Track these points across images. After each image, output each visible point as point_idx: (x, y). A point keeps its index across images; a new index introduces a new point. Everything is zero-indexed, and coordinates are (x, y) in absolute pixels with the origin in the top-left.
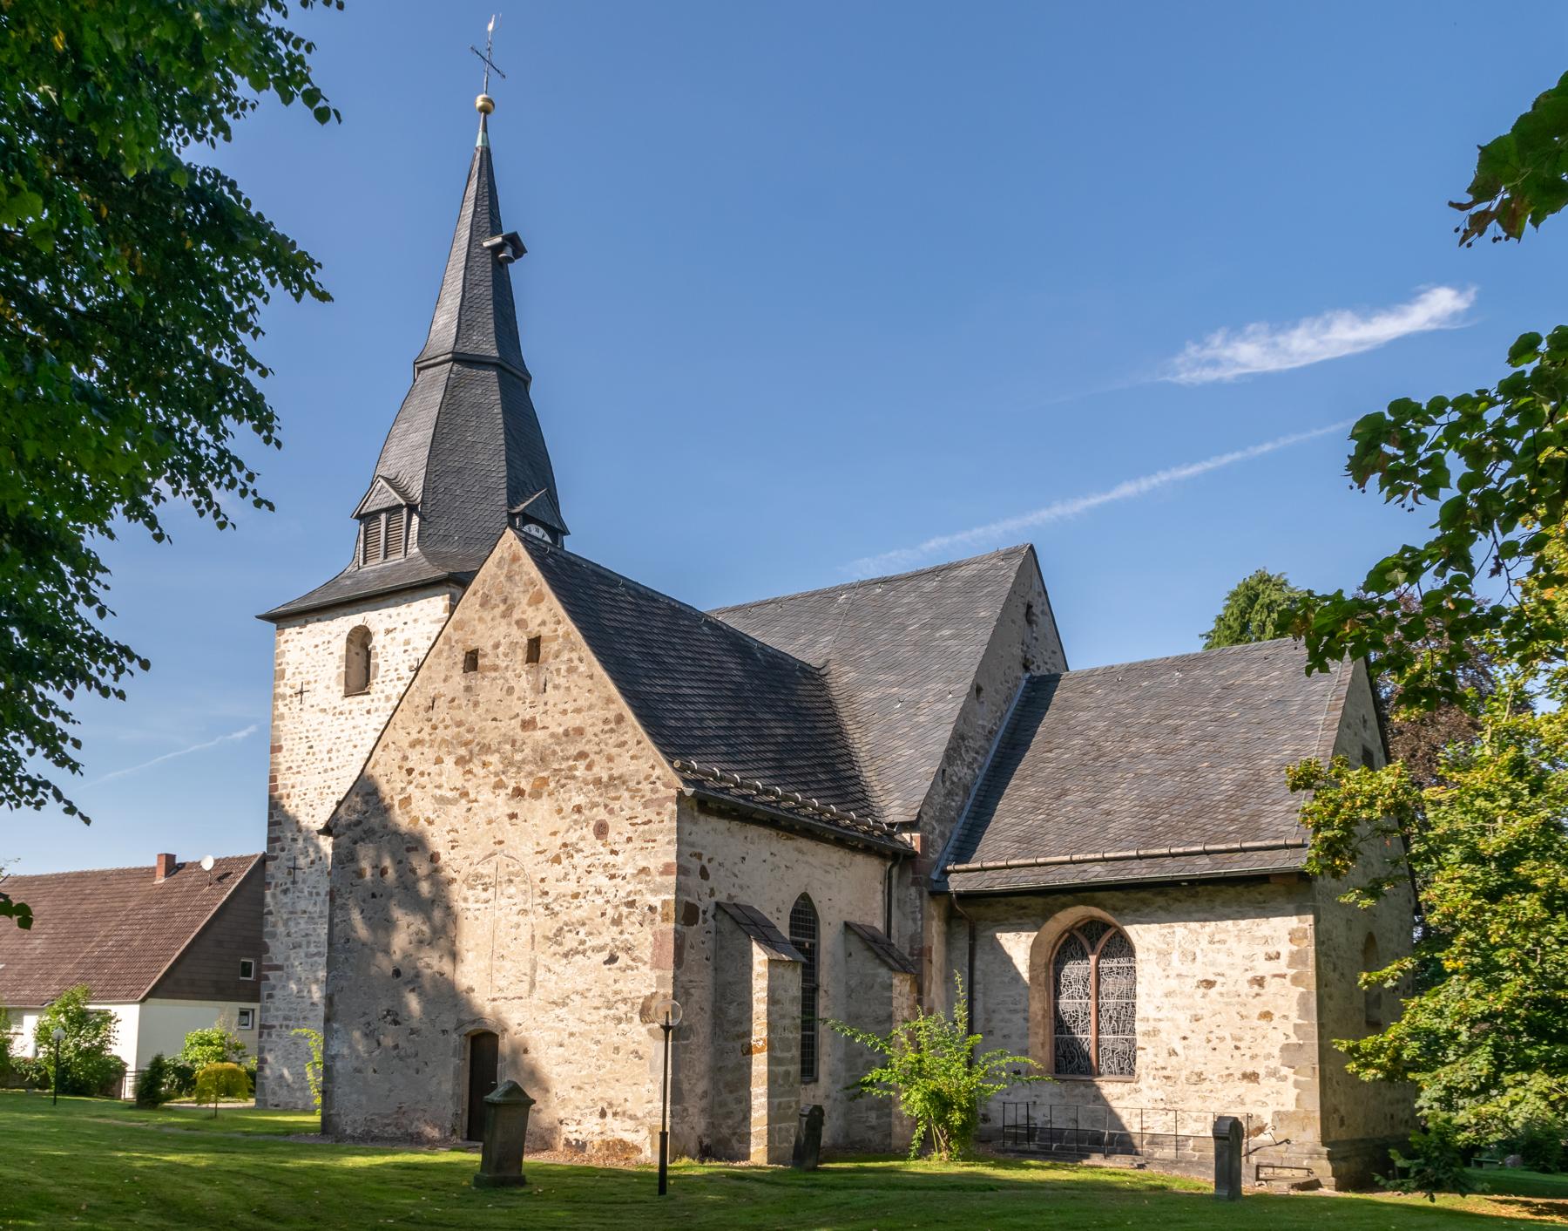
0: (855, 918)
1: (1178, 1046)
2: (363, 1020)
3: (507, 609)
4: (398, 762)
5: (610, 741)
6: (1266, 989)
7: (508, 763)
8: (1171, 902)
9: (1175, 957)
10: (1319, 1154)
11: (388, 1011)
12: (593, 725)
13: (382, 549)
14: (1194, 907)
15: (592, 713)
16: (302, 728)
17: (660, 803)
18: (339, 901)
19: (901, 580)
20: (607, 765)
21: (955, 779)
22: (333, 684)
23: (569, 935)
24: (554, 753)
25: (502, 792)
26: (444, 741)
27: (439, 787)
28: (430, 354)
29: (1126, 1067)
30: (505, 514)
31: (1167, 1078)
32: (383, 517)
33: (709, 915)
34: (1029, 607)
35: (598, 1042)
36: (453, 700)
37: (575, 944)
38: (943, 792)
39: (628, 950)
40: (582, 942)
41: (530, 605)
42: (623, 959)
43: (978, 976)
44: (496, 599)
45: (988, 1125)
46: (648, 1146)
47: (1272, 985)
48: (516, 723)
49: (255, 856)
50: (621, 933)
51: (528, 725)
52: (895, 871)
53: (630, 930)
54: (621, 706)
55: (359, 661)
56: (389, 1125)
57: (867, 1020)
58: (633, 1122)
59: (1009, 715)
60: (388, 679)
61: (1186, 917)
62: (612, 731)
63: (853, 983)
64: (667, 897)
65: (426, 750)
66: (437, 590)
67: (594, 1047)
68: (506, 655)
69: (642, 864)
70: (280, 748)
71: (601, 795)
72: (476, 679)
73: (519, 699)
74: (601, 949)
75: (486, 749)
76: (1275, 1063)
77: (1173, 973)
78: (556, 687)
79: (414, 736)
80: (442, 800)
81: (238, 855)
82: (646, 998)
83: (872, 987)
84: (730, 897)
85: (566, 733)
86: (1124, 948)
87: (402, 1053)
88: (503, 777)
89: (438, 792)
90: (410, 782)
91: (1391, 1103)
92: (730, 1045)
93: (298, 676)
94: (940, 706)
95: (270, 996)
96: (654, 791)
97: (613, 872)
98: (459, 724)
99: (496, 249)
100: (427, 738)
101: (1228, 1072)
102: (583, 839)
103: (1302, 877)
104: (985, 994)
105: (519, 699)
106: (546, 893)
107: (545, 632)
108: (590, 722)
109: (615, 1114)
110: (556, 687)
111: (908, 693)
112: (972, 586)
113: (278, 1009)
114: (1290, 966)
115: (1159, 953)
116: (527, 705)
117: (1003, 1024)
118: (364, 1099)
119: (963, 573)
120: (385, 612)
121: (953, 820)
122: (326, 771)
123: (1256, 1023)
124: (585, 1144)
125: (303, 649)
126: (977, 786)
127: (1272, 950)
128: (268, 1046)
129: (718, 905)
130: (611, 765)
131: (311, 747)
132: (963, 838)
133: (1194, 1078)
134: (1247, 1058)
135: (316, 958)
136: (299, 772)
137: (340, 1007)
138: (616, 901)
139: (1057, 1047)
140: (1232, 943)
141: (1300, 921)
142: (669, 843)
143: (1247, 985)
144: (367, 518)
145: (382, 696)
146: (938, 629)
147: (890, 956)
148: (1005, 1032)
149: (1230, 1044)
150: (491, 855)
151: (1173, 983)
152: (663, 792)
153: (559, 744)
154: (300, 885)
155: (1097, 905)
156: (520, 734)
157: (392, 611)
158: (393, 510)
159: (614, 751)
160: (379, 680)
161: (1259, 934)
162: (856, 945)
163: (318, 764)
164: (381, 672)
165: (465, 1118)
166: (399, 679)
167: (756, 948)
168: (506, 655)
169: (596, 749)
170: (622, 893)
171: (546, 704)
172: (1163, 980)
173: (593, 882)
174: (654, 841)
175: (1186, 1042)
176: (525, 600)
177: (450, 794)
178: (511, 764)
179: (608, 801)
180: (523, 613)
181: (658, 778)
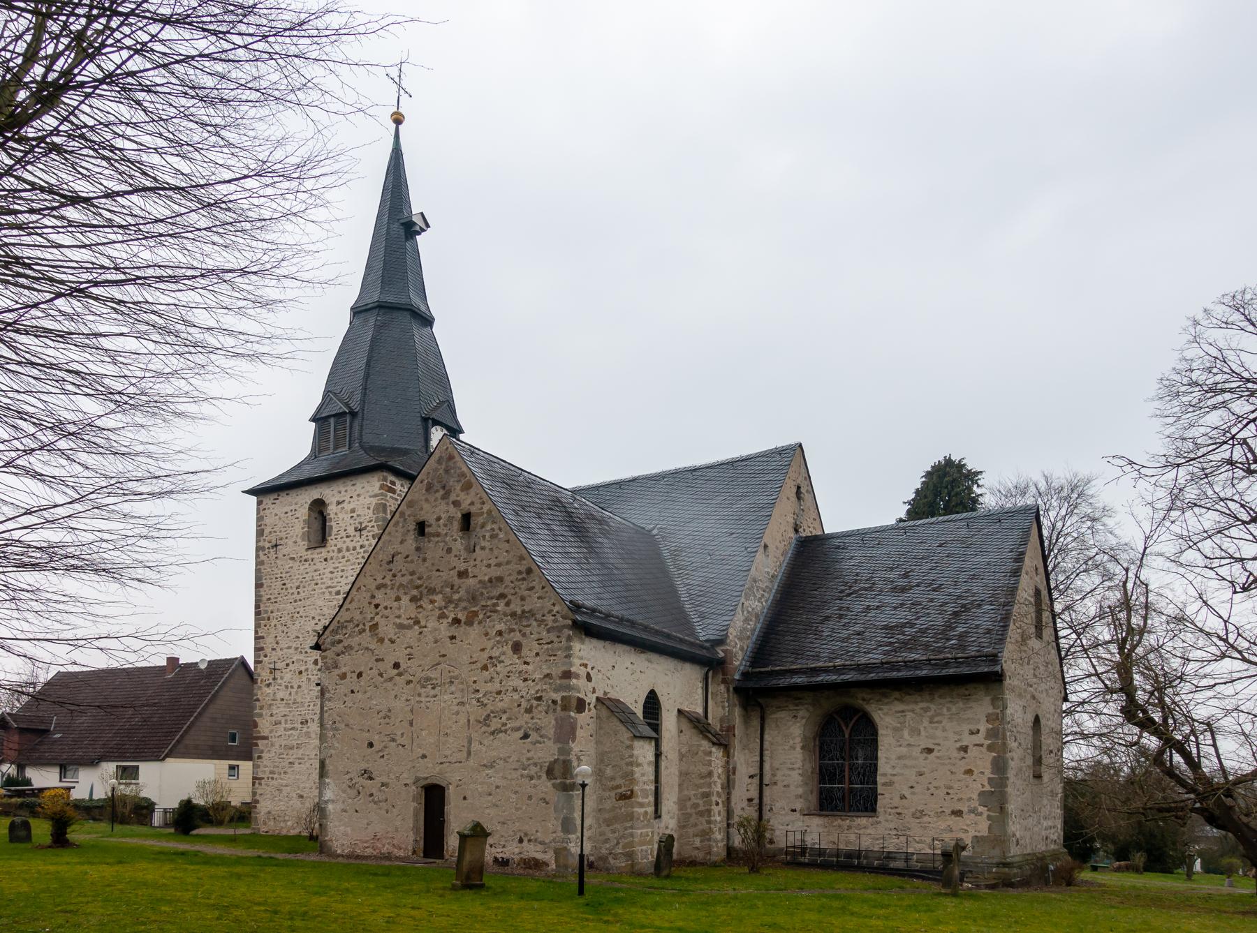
1: (907, 793)
2: (347, 777)
4: (368, 599)
7: (449, 601)
11: (365, 771)
12: (510, 575)
14: (919, 699)
16: (276, 571)
17: (560, 629)
21: (750, 609)
22: (299, 540)
23: (495, 720)
24: (482, 594)
25: (445, 621)
26: (401, 585)
27: (399, 617)
31: (899, 814)
32: (332, 420)
33: (592, 706)
34: (799, 488)
35: (516, 792)
36: (407, 557)
37: (499, 726)
38: (742, 618)
39: (537, 730)
40: (504, 725)
41: (462, 490)
42: (534, 736)
43: (766, 745)
44: (437, 486)
45: (773, 846)
47: (974, 751)
48: (454, 573)
50: (532, 718)
51: (463, 574)
52: (710, 674)
55: (317, 525)
60: (339, 537)
62: (524, 579)
65: (388, 591)
67: (514, 796)
68: (445, 525)
71: (516, 624)
73: (456, 556)
74: (518, 729)
75: (432, 591)
76: (975, 804)
78: (483, 548)
79: (380, 581)
80: (401, 627)
82: (550, 762)
83: (697, 753)
84: (605, 693)
85: (490, 580)
87: (376, 799)
89: (398, 621)
90: (377, 614)
91: (1046, 829)
95: (260, 757)
100: (389, 583)
102: (504, 653)
104: (771, 757)
106: (478, 691)
107: (473, 509)
108: (507, 573)
109: (530, 841)
110: (483, 548)
113: (266, 766)
116: (462, 560)
118: (349, 829)
121: (748, 638)
122: (295, 601)
124: (508, 860)
127: (974, 728)
128: (259, 792)
129: (598, 699)
130: (523, 603)
131: (284, 584)
137: (330, 767)
139: (821, 793)
143: (956, 751)
145: (335, 549)
147: (709, 732)
148: (785, 783)
151: (904, 750)
152: (561, 622)
154: (279, 681)
156: (457, 581)
160: (333, 537)
162: (685, 725)
163: (289, 596)
164: (334, 531)
165: (422, 843)
168: (445, 525)
169: (513, 591)
173: (511, 683)
176: (458, 487)
177: (406, 622)
178: (450, 601)
179: (522, 628)
180: (457, 496)
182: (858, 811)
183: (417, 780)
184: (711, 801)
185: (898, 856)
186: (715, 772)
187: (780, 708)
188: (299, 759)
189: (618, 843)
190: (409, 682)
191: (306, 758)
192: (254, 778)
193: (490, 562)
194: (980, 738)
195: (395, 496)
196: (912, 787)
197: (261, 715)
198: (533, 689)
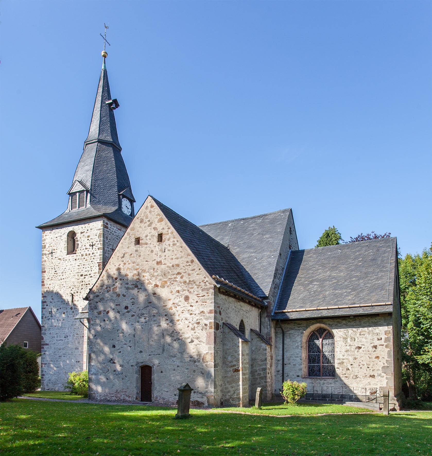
0: (253, 328)
3: (150, 224)
5: (189, 269)
6: (377, 349)
8: (347, 322)
9: (349, 340)
10: (394, 399)
12: (183, 263)
13: (78, 205)
15: (182, 259)
17: (208, 289)
18: (92, 322)
19: (249, 219)
20: (188, 277)
21: (276, 283)
22: (63, 250)
24: (169, 273)
28: (90, 139)
29: (331, 374)
30: (117, 194)
32: (78, 194)
34: (290, 228)
35: (187, 369)
36: (131, 254)
41: (158, 222)
46: (206, 402)
47: (379, 348)
48: (155, 263)
49: (27, 308)
50: (195, 333)
51: (159, 263)
53: (198, 332)
54: (193, 257)
55: (71, 243)
56: (113, 396)
57: (258, 360)
58: (201, 395)
59: (287, 263)
60: (82, 249)
61: (353, 326)
62: (190, 265)
63: (253, 349)
64: (211, 321)
66: (99, 219)
67: (186, 371)
69: (202, 310)
70: (45, 272)
71: (186, 287)
72: (139, 247)
73: (155, 254)
76: (380, 372)
77: (348, 345)
78: (169, 250)
81: (21, 307)
85: (173, 266)
86: (331, 336)
87: (117, 373)
88: (150, 281)
89: (127, 286)
92: (229, 369)
93: (50, 247)
94: (270, 259)
96: (206, 285)
97: (191, 312)
98: (134, 263)
99: (110, 104)
101: (365, 375)
102: (180, 301)
103: (390, 314)
105: (155, 254)
107: (164, 232)
108: (181, 262)
110: (169, 250)
111: (259, 256)
112: (273, 222)
114: (385, 342)
115: (344, 338)
116: (158, 256)
117: (293, 361)
119: (269, 217)
120: (80, 226)
122: (61, 279)
123: (374, 359)
125: (52, 238)
126: (281, 286)
127: (379, 338)
129: (223, 323)
130: (190, 277)
131: (56, 271)
132: (279, 302)
133: (355, 377)
134: (371, 370)
135: (60, 341)
136: (52, 280)
138: (193, 322)
139: (309, 368)
140: (367, 335)
141: (388, 328)
142: (211, 303)
144: (72, 195)
146: (265, 235)
148: (294, 363)
149: (366, 366)
150: (147, 307)
151: (348, 348)
152: (209, 286)
153: (171, 270)
155: (324, 323)
156: (156, 266)
157: (83, 226)
158: (81, 192)
159: (191, 272)
160: (79, 249)
161: (375, 332)
163: (58, 277)
164: (80, 246)
165: (140, 394)
166: (86, 249)
167: (240, 339)
168: (150, 239)
169: (184, 271)
170: (195, 320)
171: (165, 256)
172: (345, 347)
174: (206, 302)
175: (352, 366)
177: (131, 287)
180: (156, 225)
181: (207, 281)
182: (326, 376)
183: (138, 363)
184: (266, 372)
185: (346, 397)
186: (268, 358)
187: (292, 329)
188: (64, 354)
189: (234, 393)
190: (133, 316)
191: (67, 353)
193: (173, 257)
194: (382, 342)
195: (108, 230)
196: (352, 365)
197: (45, 334)
198: (195, 318)
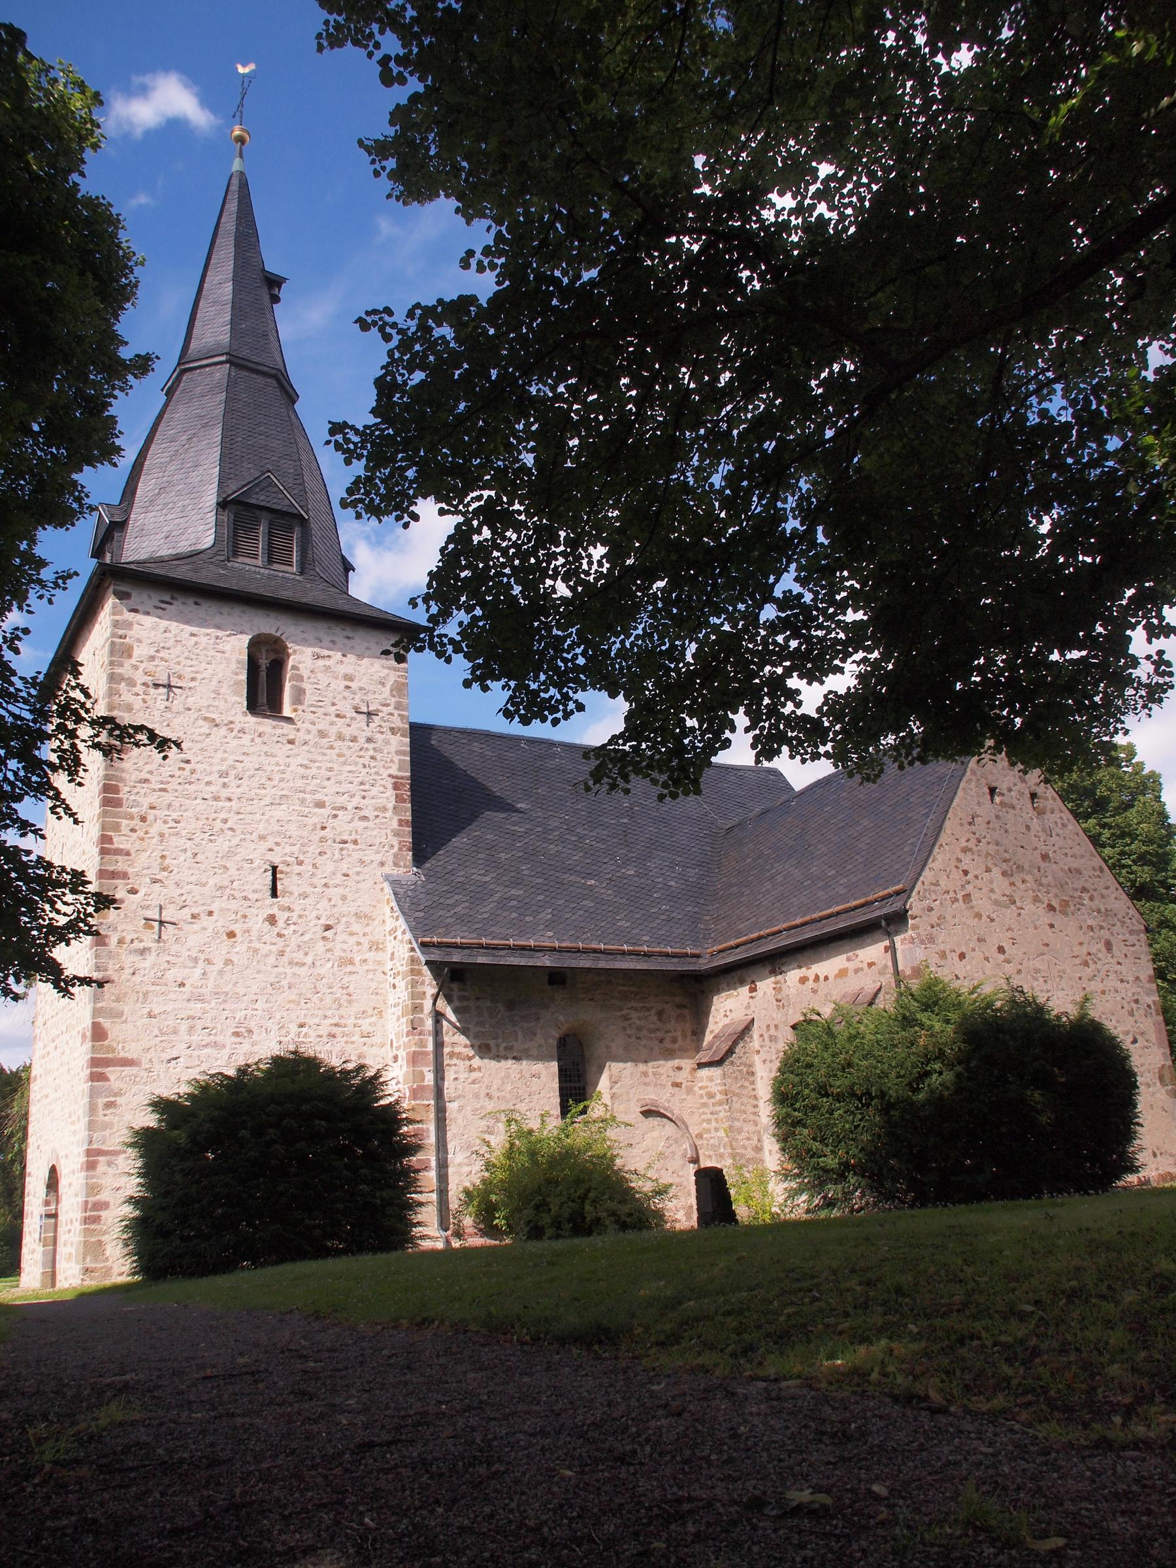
122: (216, 799)
192: (89, 1153)
